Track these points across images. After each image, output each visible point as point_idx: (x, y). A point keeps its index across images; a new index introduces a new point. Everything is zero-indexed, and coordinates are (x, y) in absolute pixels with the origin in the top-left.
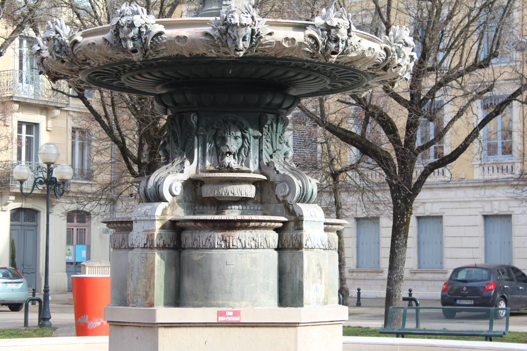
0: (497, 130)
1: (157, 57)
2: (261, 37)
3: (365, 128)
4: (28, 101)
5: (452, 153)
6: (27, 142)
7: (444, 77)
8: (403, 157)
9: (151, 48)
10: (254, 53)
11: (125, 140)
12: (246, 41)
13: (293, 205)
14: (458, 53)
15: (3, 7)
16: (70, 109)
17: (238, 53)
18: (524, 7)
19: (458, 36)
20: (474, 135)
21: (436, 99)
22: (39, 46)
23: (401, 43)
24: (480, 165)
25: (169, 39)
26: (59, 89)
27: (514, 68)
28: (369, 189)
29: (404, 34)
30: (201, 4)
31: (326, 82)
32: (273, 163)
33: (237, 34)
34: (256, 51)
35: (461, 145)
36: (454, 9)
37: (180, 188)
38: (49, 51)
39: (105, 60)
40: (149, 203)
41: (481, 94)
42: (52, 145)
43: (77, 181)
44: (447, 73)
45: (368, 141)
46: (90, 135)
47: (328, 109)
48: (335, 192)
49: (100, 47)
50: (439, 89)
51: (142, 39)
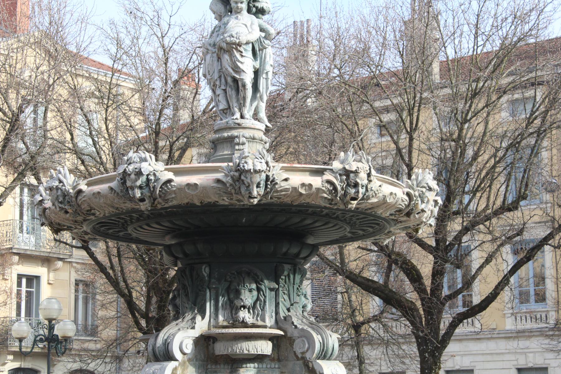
0: (528, 276)
1: (166, 205)
2: (276, 183)
3: (388, 276)
4: (28, 253)
5: (482, 302)
6: (26, 297)
7: (470, 221)
8: (429, 307)
9: (160, 196)
10: (269, 200)
11: (132, 292)
12: (260, 187)
13: (313, 362)
14: (485, 195)
15: (3, 155)
16: (73, 260)
17: (252, 200)
18: (553, 146)
19: (484, 178)
20: (504, 282)
21: (463, 244)
22: (41, 196)
23: (424, 187)
24: (512, 314)
25: (179, 187)
26: (62, 240)
27: (544, 210)
28: (394, 341)
29: (427, 178)
30: (212, 149)
31: (345, 229)
32: (291, 317)
33: (251, 180)
34: (271, 198)
35: (491, 293)
36: (479, 149)
37: (192, 346)
38: (52, 201)
39: (111, 209)
40: (158, 363)
41: (510, 238)
42: (53, 300)
43: (80, 338)
44: (474, 217)
45: (391, 291)
46: (95, 288)
47: (348, 255)
48: (357, 345)
49: (105, 196)
50: (466, 233)
51: (150, 187)
